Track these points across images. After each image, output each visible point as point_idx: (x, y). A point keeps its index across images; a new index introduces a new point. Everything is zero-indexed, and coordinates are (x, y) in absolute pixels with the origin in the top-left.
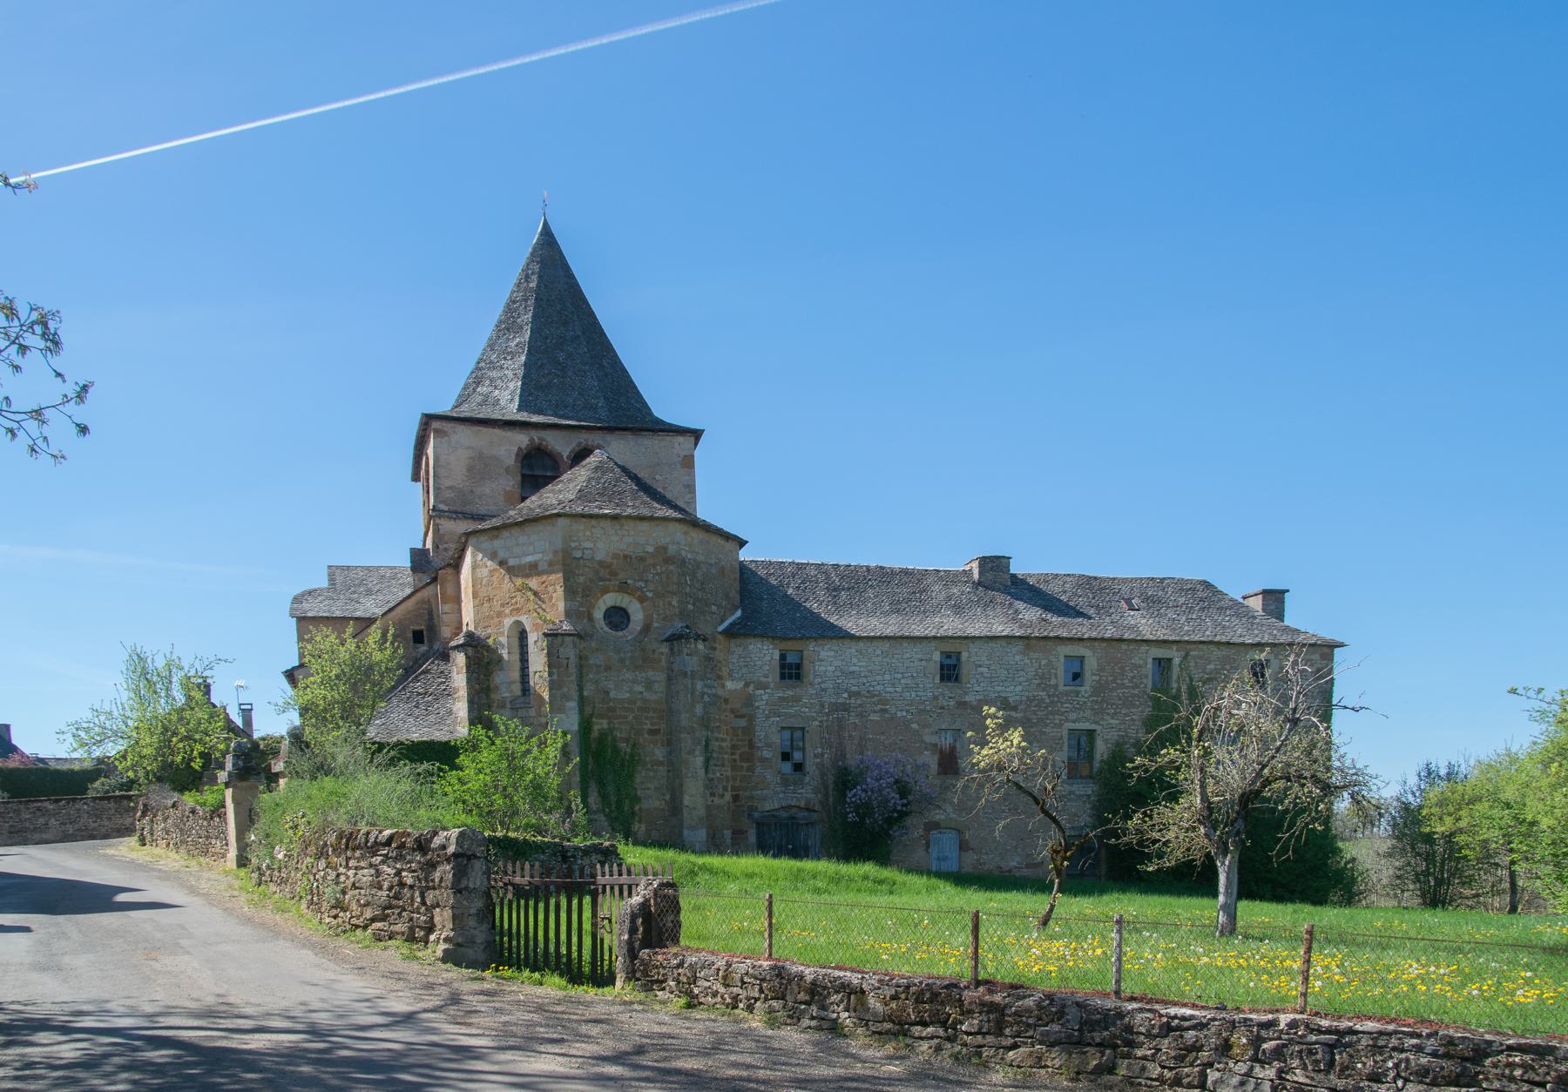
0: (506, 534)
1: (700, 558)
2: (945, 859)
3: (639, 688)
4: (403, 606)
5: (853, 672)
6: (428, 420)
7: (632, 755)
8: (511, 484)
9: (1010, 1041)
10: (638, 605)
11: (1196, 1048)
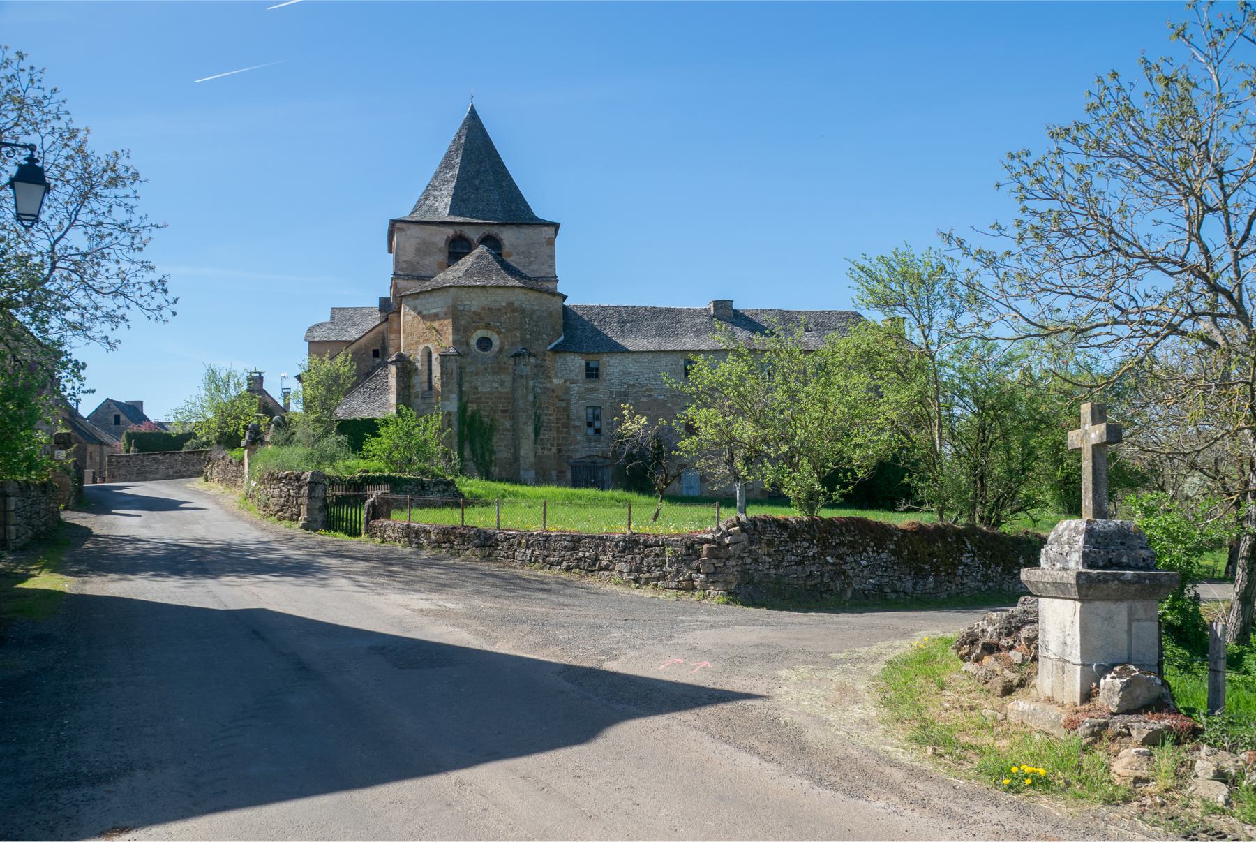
0: (422, 296)
1: (536, 308)
2: (692, 487)
3: (496, 385)
4: (366, 336)
5: (630, 373)
6: (394, 223)
7: (490, 425)
9: (466, 547)
10: (496, 336)
11: (513, 545)
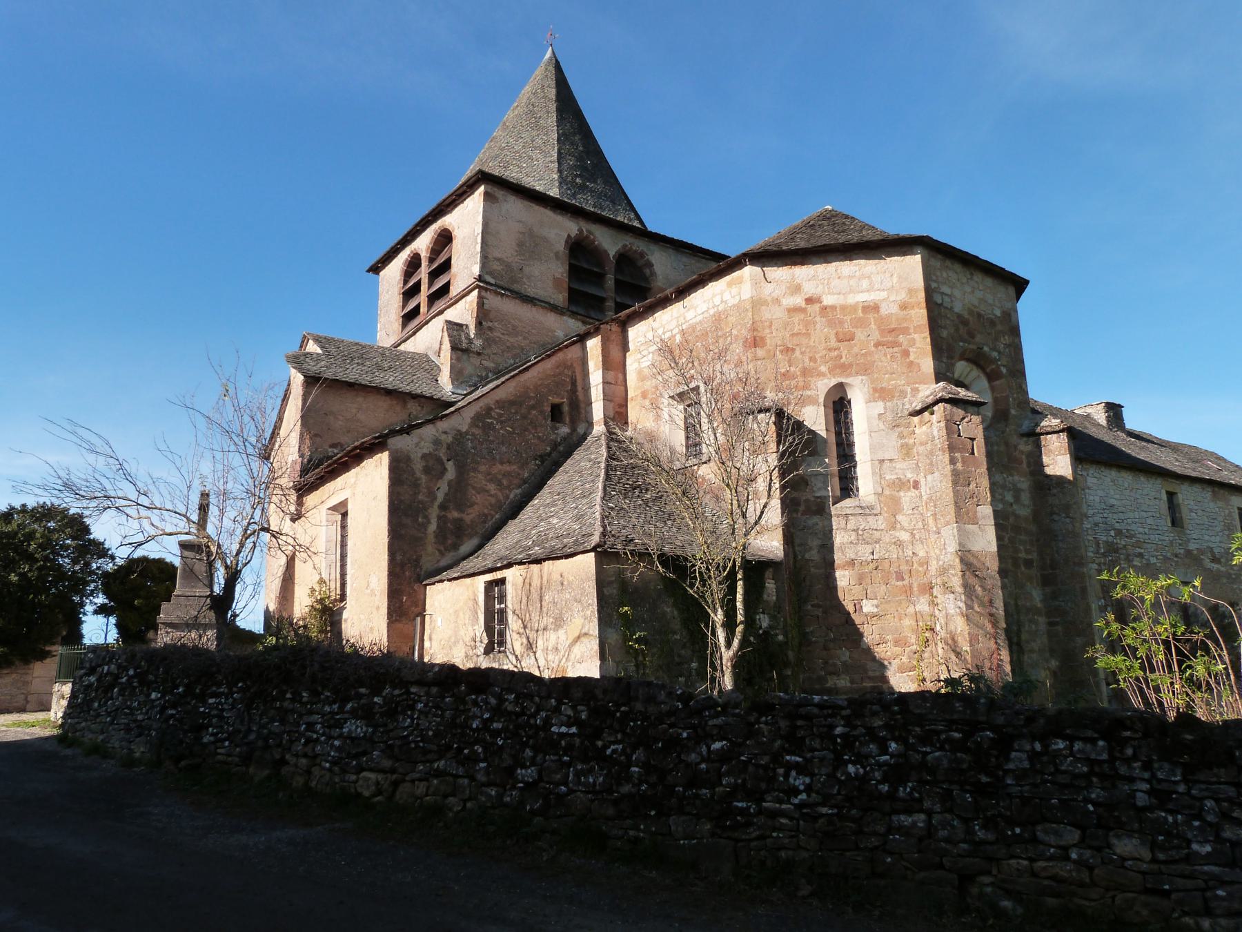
8: (560, 270)
